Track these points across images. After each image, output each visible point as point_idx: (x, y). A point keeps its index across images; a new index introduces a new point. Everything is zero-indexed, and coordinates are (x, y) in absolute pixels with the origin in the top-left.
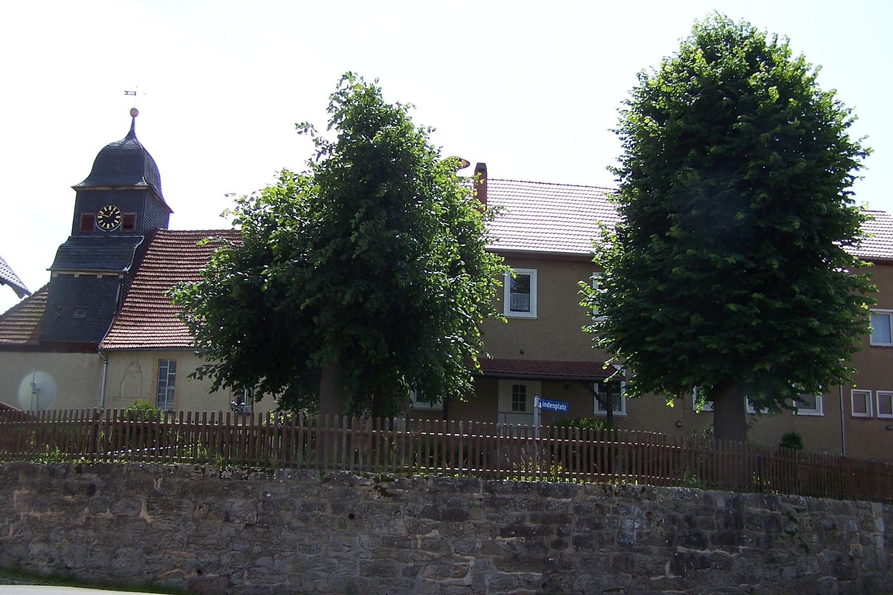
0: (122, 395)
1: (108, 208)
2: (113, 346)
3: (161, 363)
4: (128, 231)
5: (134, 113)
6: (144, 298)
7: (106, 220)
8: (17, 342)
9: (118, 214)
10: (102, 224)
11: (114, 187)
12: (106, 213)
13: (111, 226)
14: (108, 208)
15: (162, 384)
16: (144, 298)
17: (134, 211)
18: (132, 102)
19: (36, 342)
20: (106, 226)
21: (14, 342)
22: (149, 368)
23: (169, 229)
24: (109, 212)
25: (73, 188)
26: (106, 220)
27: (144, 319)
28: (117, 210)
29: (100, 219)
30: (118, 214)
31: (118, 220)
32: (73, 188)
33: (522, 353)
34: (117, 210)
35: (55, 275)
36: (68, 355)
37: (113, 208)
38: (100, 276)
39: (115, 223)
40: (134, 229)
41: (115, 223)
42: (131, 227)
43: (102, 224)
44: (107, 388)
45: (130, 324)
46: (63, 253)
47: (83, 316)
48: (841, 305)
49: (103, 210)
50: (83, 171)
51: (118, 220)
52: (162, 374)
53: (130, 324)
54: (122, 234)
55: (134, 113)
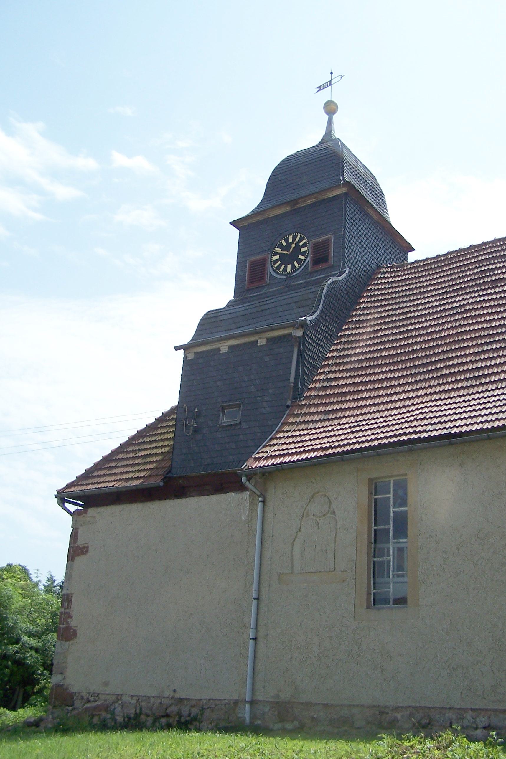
1: (287, 240)
3: (375, 487)
4: (320, 267)
5: (330, 109)
7: (285, 260)
9: (304, 245)
10: (279, 267)
11: (295, 202)
13: (293, 267)
14: (287, 240)
15: (377, 537)
18: (325, 96)
19: (158, 481)
20: (285, 269)
21: (124, 484)
22: (348, 498)
23: (409, 261)
24: (289, 245)
25: (234, 223)
28: (301, 239)
30: (304, 245)
31: (303, 254)
32: (234, 223)
34: (301, 239)
35: (190, 357)
36: (214, 498)
37: (294, 238)
38: (262, 342)
40: (331, 261)
41: (299, 261)
43: (279, 267)
44: (267, 554)
46: (210, 322)
49: (281, 246)
50: (249, 197)
51: (303, 254)
52: (377, 512)
53: (316, 418)
55: (330, 109)
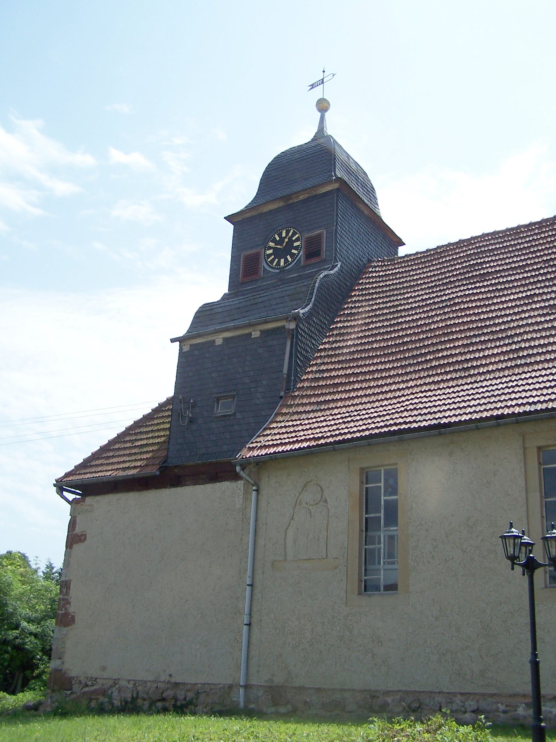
1: (280, 235)
3: (367, 476)
4: (313, 261)
5: (323, 106)
7: (278, 254)
11: (288, 197)
13: (286, 261)
14: (280, 235)
15: (369, 525)
18: (317, 94)
19: (154, 470)
20: (279, 263)
24: (282, 239)
25: (228, 218)
27: (338, 397)
28: (294, 234)
31: (296, 248)
32: (228, 218)
33: (171, 675)
34: (294, 234)
35: (186, 349)
36: (209, 487)
39: (292, 255)
40: (323, 256)
41: (292, 255)
44: (261, 542)
45: (308, 408)
46: (206, 315)
49: (274, 241)
50: (243, 192)
51: (296, 248)
52: (368, 501)
53: (308, 408)
55: (323, 106)
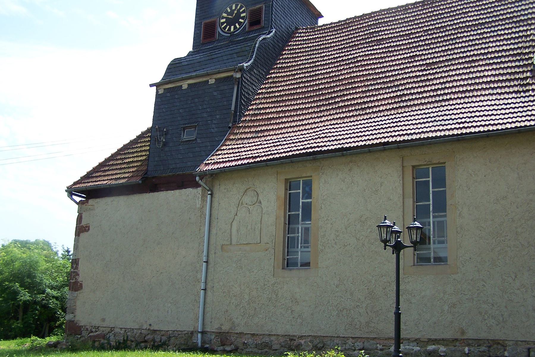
0: (234, 242)
1: (231, 8)
2: (216, 166)
4: (255, 28)
6: (272, 102)
7: (230, 22)
8: (117, 182)
12: (228, 14)
13: (235, 27)
14: (231, 8)
15: (291, 221)
16: (272, 102)
17: (260, 3)
20: (230, 29)
21: (114, 182)
22: (270, 195)
23: (319, 25)
26: (230, 22)
29: (223, 23)
31: (243, 18)
36: (177, 192)
38: (212, 81)
39: (240, 23)
41: (240, 23)
42: (258, 22)
44: (214, 231)
45: (249, 136)
46: (176, 67)
47: (193, 137)
48: (347, 311)
49: (226, 12)
51: (243, 18)
52: (291, 202)
53: (249, 136)
54: (249, 32)
